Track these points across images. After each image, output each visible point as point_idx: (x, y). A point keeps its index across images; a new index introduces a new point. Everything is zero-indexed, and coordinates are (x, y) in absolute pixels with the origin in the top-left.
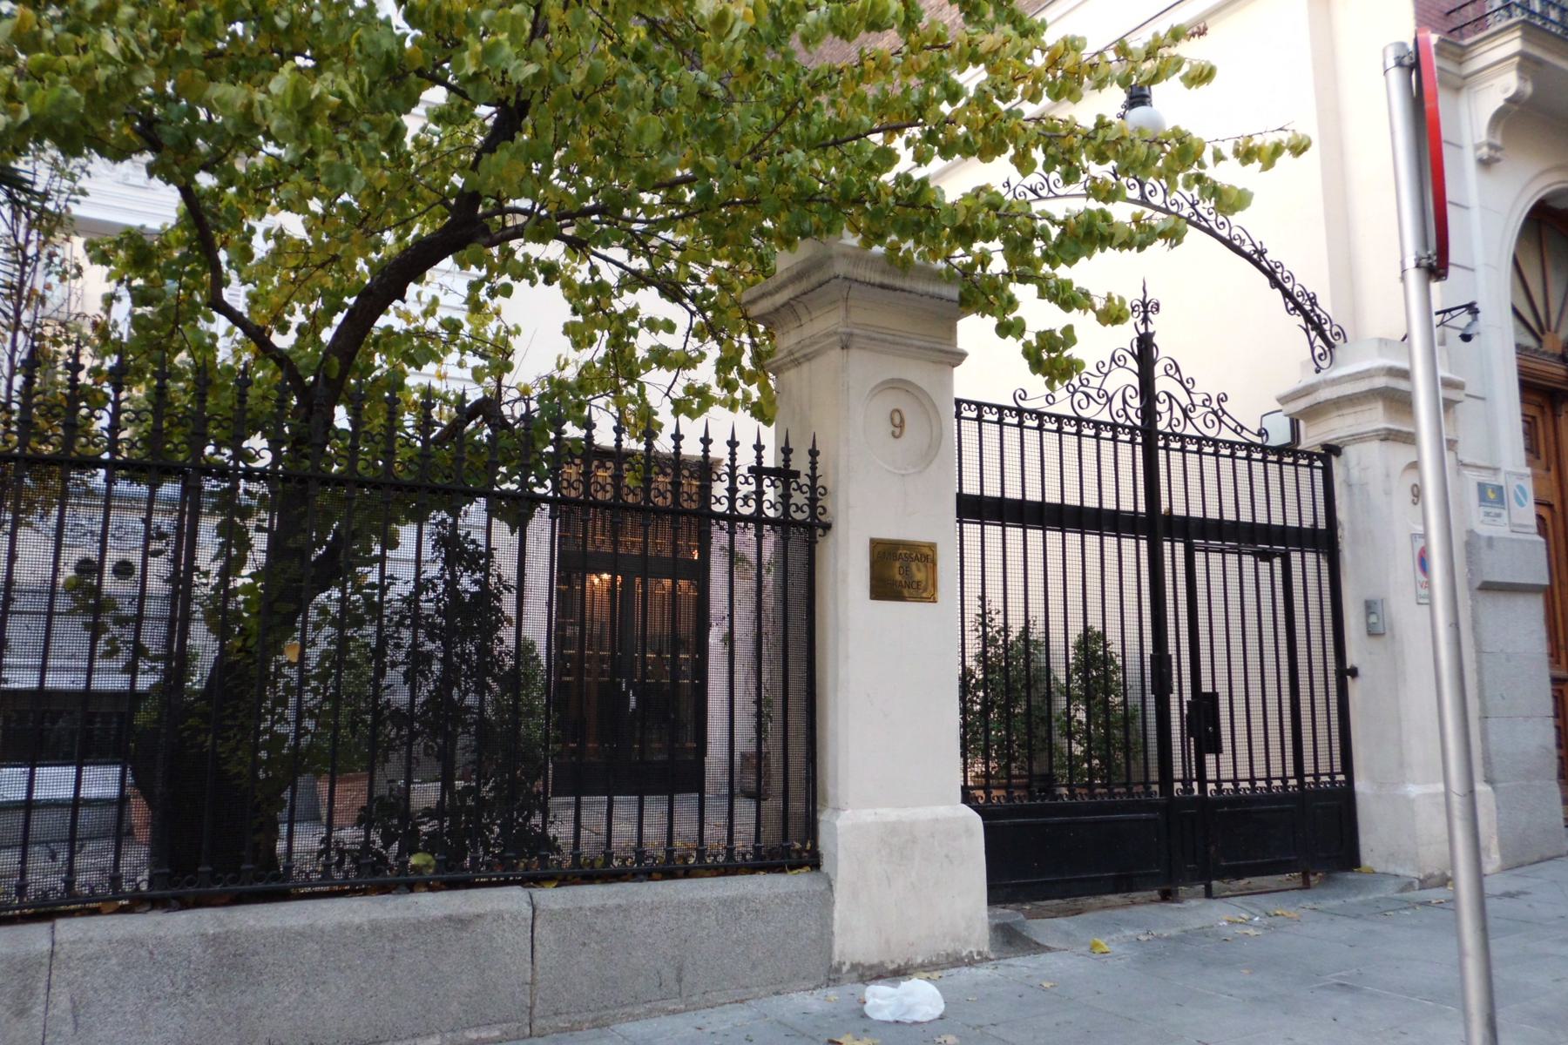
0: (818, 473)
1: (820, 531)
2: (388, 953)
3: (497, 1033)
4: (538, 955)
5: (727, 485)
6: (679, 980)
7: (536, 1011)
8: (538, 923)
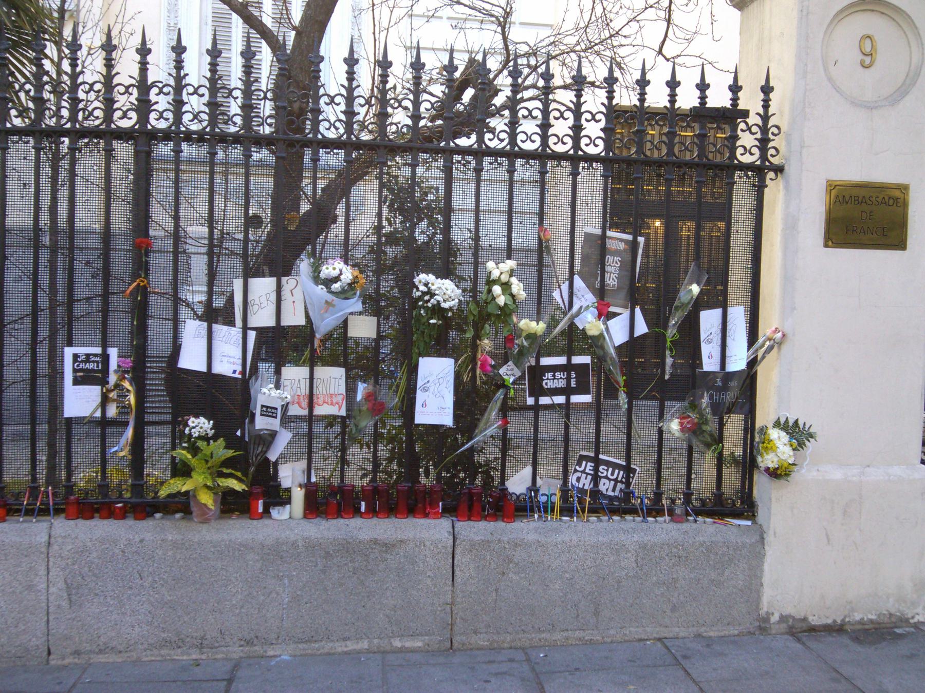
0: (771, 111)
1: (771, 175)
2: (320, 566)
3: (420, 644)
4: (458, 579)
5: (571, 122)
6: (596, 613)
7: (456, 628)
8: (458, 551)
